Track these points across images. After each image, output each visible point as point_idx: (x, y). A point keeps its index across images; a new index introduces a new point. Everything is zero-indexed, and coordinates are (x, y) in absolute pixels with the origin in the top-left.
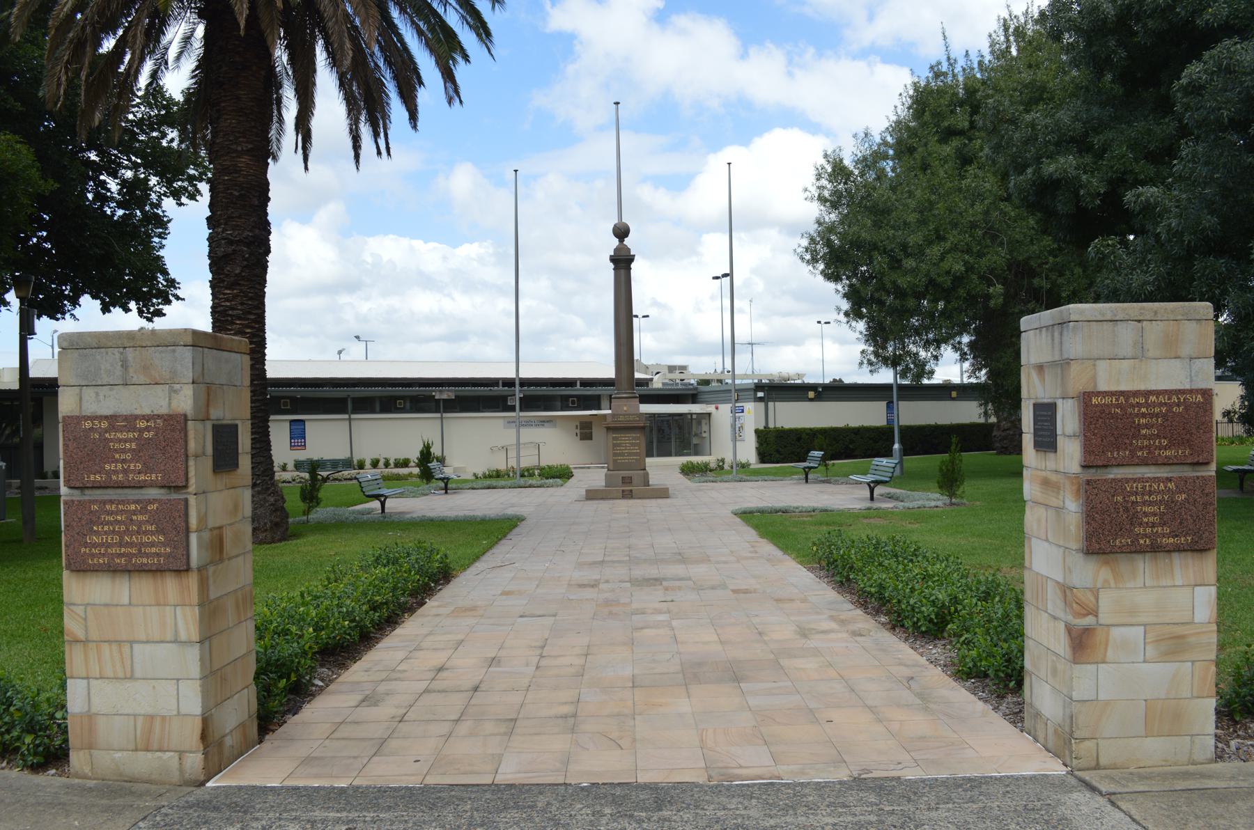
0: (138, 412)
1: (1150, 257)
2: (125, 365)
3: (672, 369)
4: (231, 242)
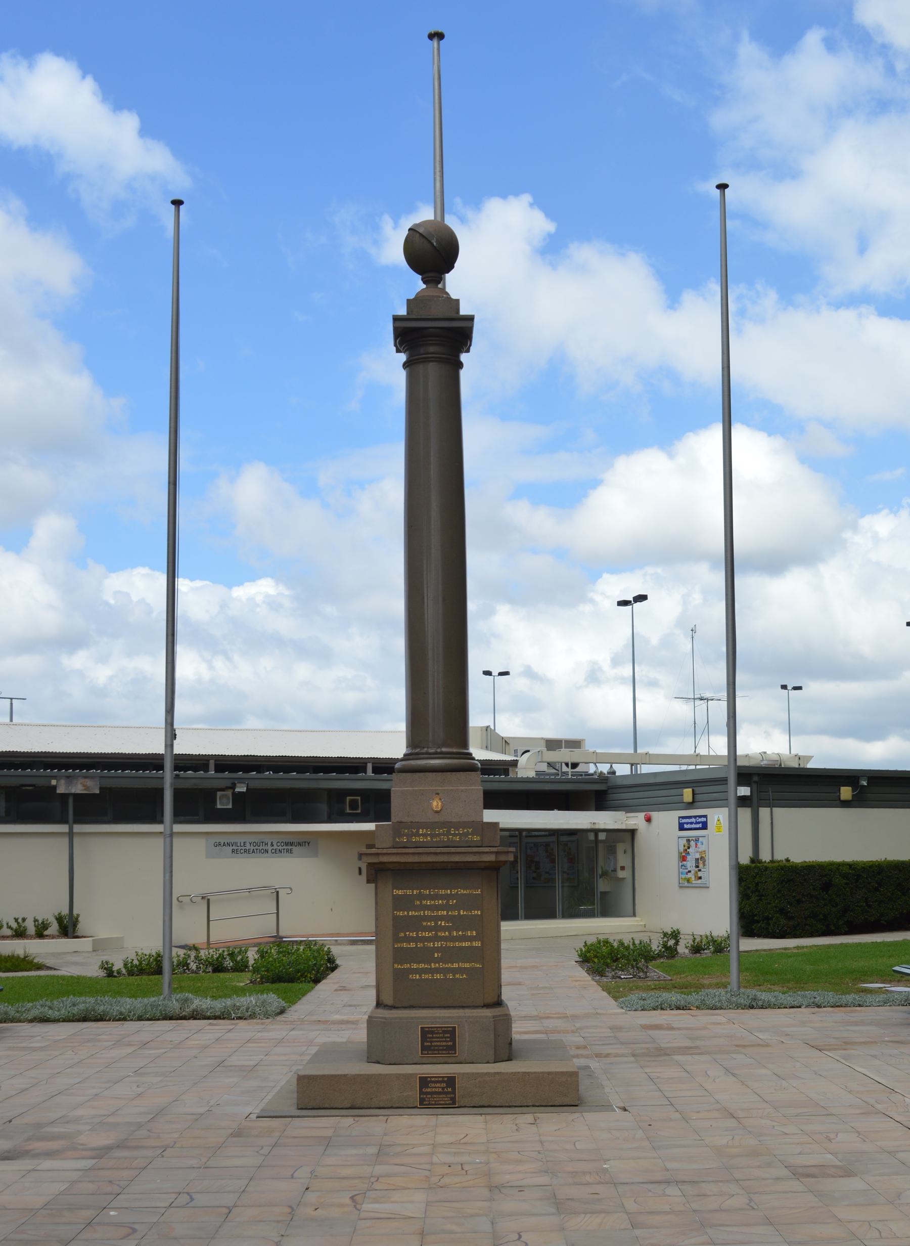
3: (552, 744)
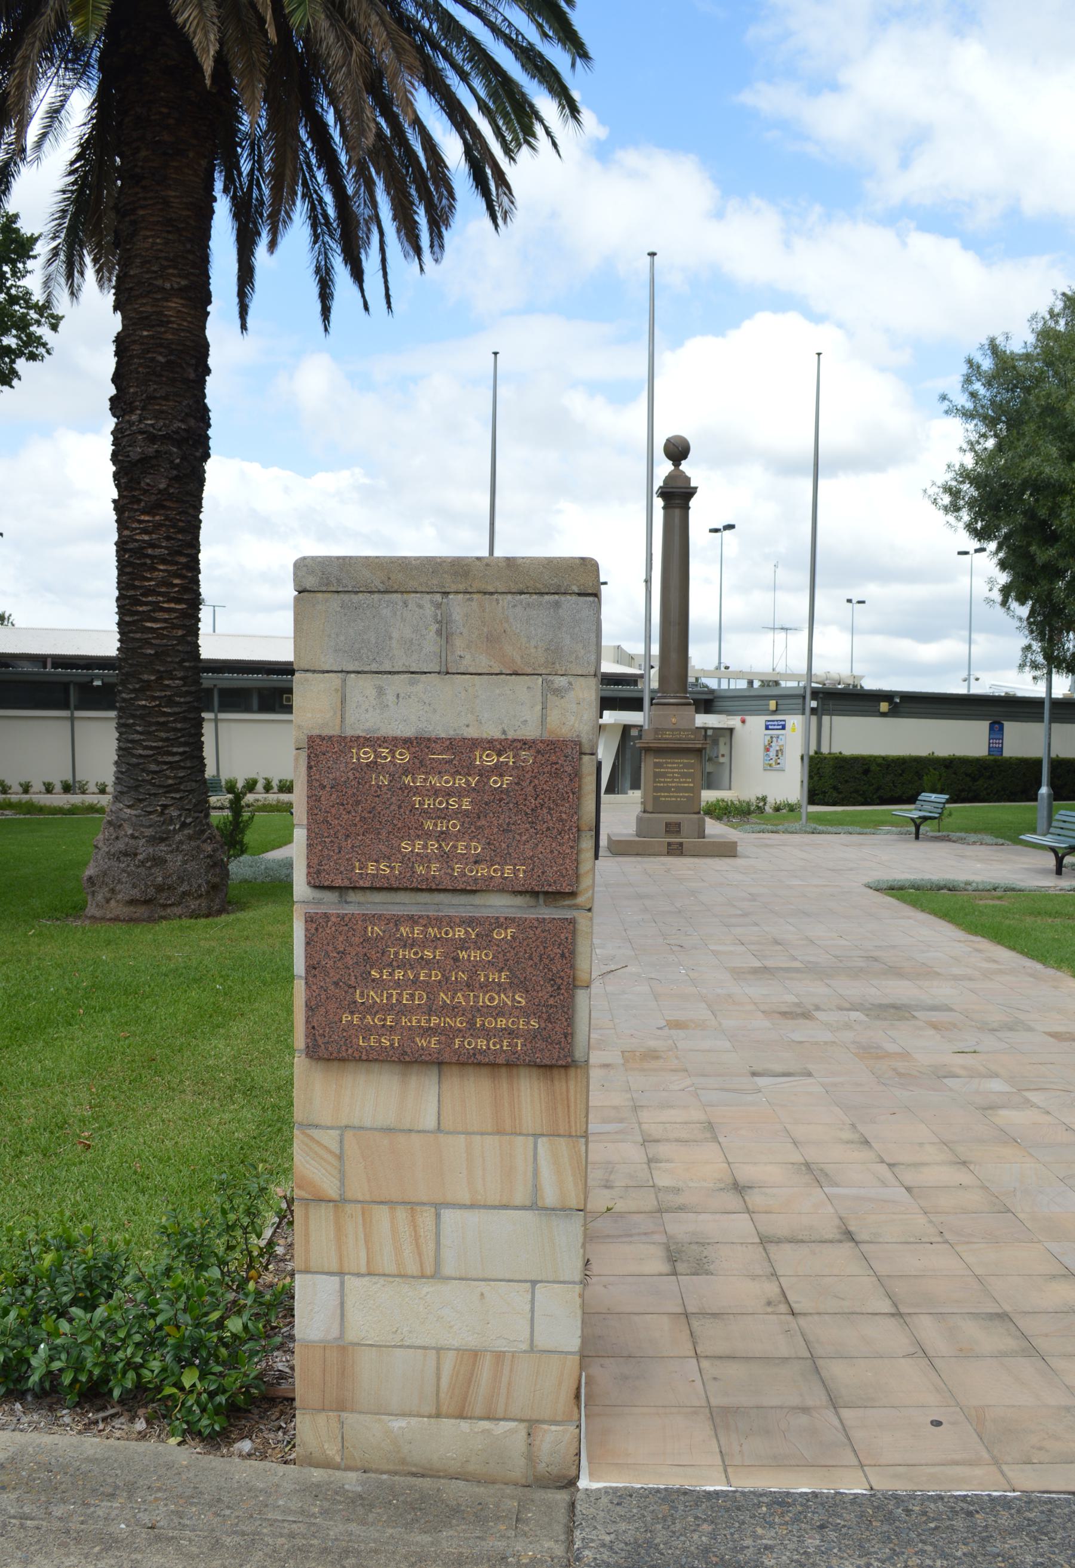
0: (472, 733)
2: (445, 630)
4: (152, 439)
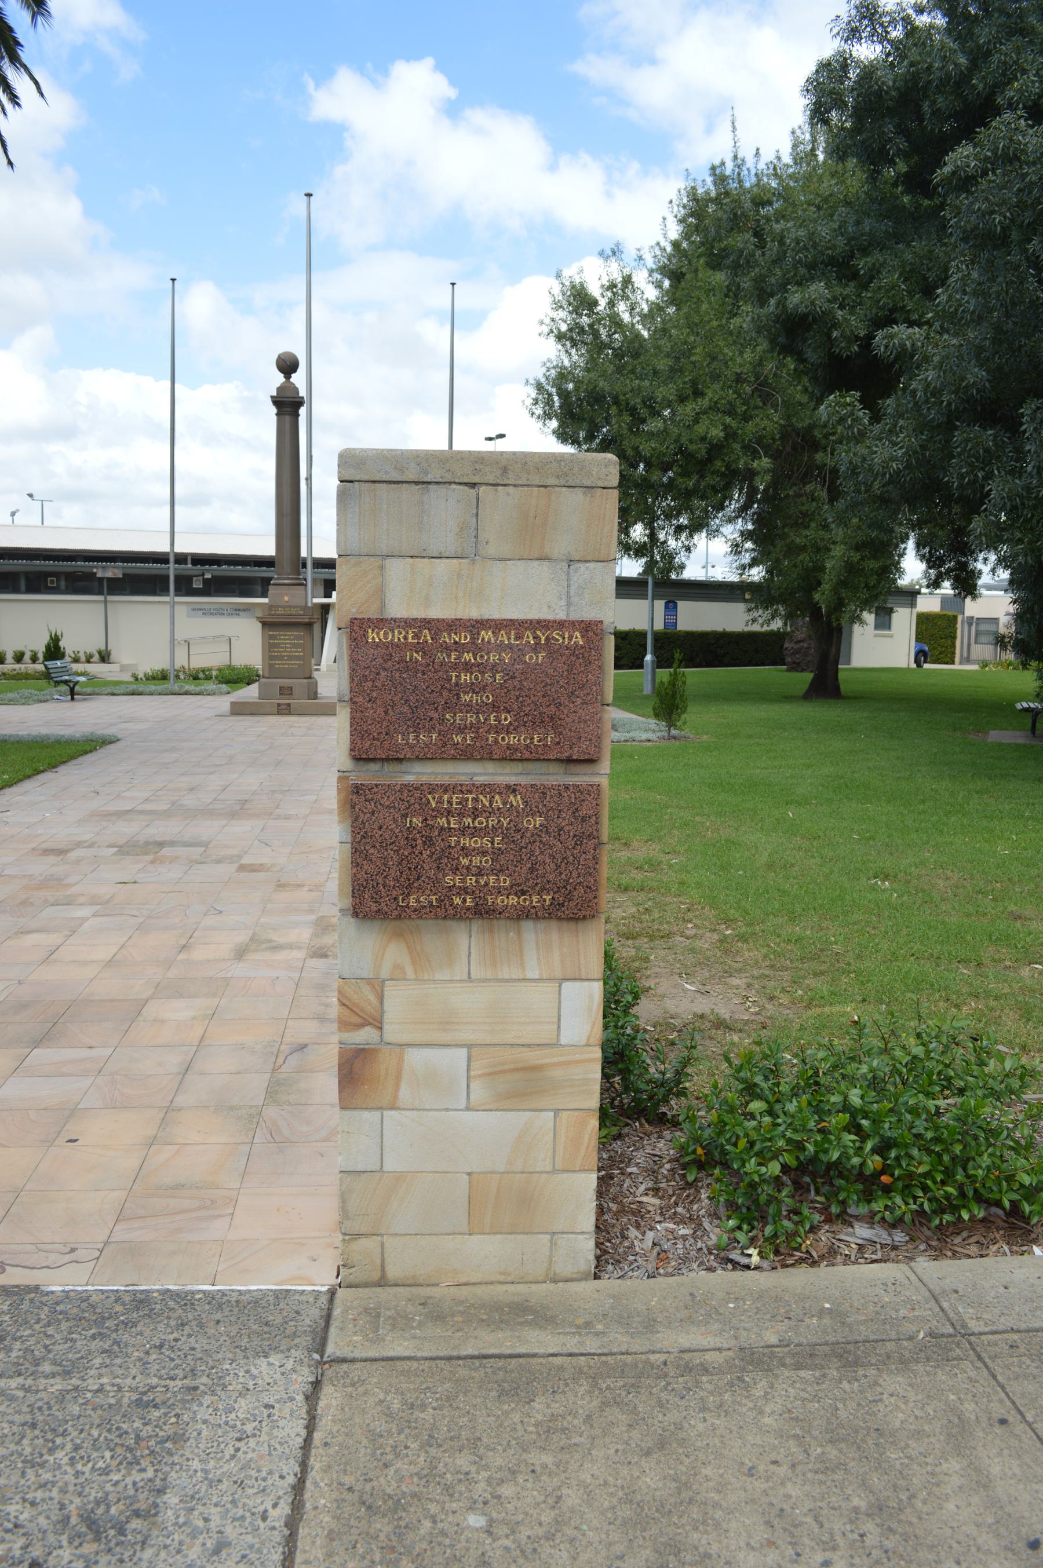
1: (901, 422)
